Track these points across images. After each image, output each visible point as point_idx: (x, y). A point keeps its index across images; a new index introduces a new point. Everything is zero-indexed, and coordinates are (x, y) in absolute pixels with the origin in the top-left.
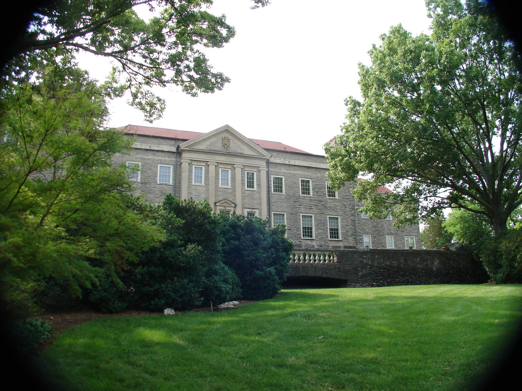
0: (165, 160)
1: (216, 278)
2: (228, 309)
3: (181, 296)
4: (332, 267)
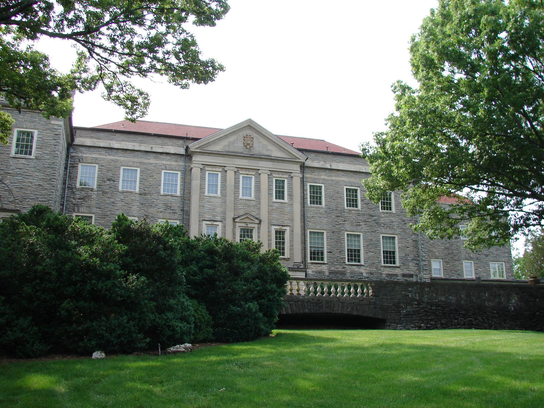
0: (171, 165)
1: (170, 315)
2: (175, 353)
3: (119, 336)
4: (365, 302)
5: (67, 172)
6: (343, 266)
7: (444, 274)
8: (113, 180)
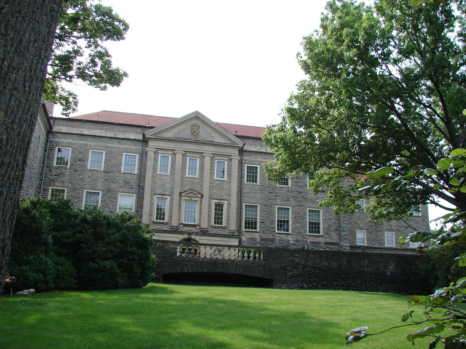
0: (131, 148)
1: (26, 267)
5: (46, 153)
6: (273, 234)
7: (367, 243)
8: (83, 160)
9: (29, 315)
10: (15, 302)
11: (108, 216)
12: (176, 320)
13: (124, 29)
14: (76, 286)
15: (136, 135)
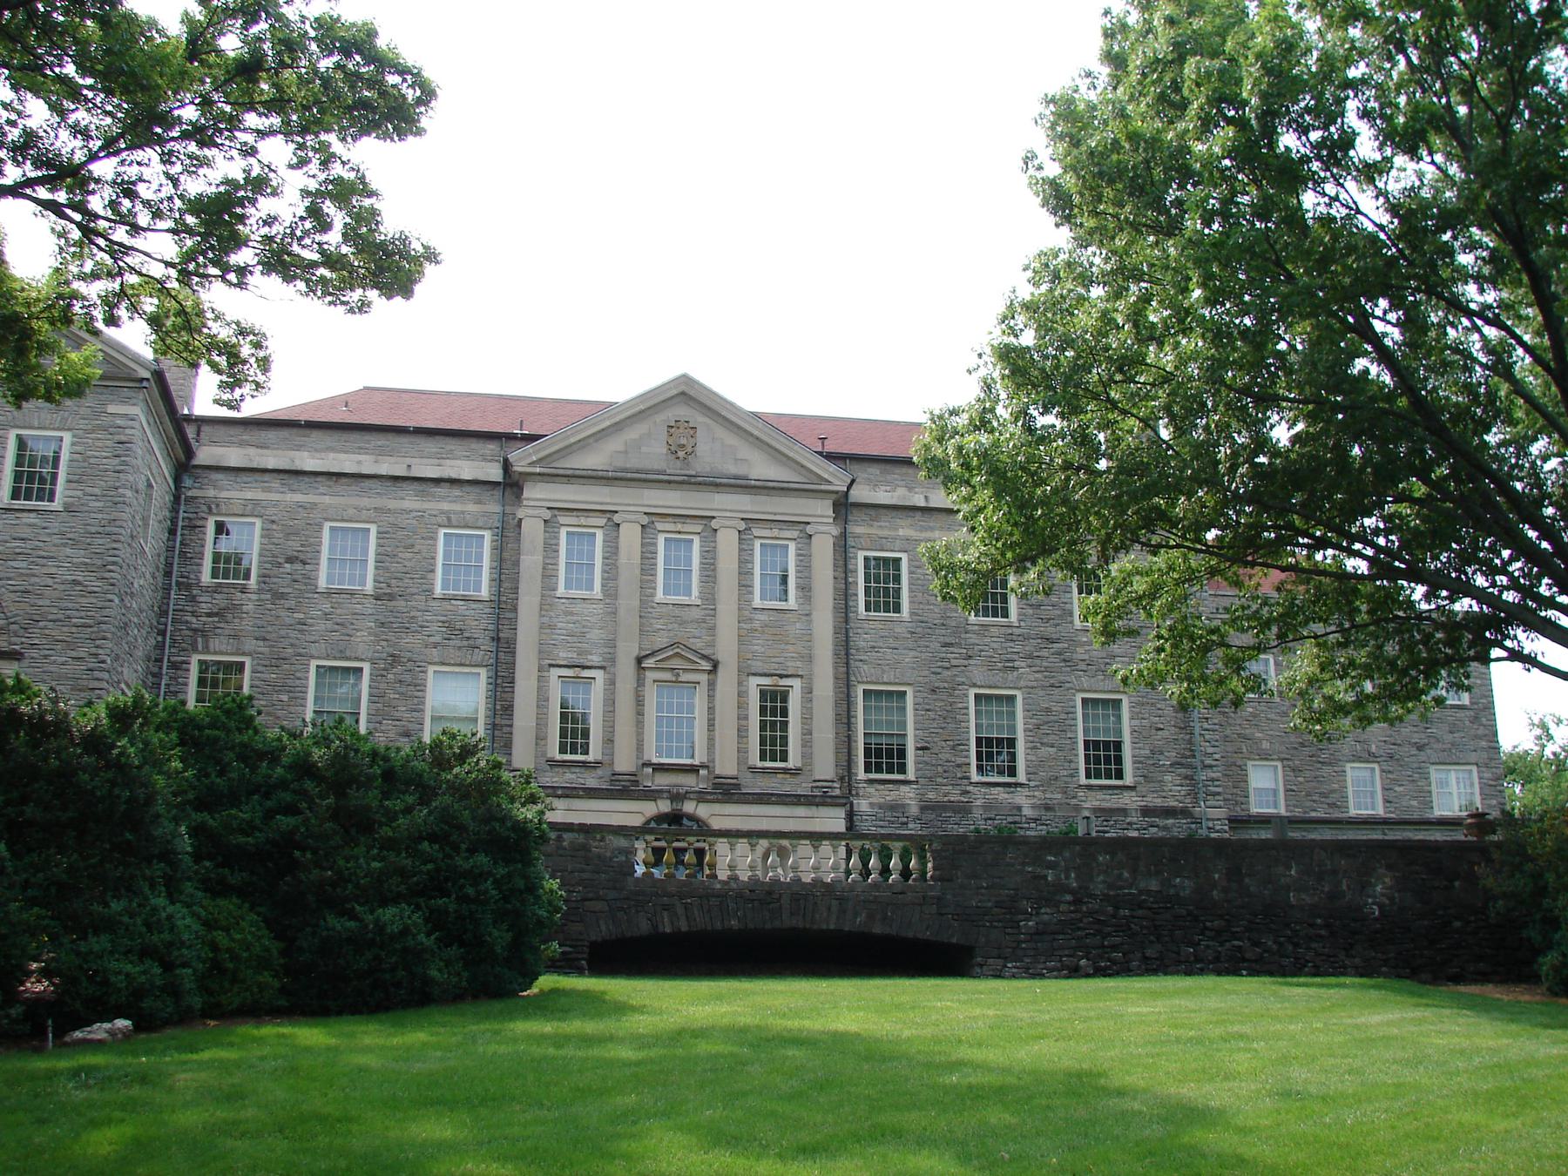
0: (463, 512)
5: (175, 541)
6: (963, 788)
7: (1287, 806)
8: (303, 559)
9: (94, 1124)
10: (51, 1075)
11: (388, 749)
12: (634, 1123)
13: (419, 102)
14: (283, 1002)
15: (480, 466)
